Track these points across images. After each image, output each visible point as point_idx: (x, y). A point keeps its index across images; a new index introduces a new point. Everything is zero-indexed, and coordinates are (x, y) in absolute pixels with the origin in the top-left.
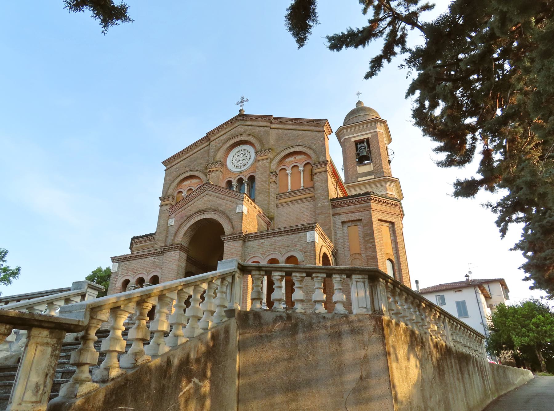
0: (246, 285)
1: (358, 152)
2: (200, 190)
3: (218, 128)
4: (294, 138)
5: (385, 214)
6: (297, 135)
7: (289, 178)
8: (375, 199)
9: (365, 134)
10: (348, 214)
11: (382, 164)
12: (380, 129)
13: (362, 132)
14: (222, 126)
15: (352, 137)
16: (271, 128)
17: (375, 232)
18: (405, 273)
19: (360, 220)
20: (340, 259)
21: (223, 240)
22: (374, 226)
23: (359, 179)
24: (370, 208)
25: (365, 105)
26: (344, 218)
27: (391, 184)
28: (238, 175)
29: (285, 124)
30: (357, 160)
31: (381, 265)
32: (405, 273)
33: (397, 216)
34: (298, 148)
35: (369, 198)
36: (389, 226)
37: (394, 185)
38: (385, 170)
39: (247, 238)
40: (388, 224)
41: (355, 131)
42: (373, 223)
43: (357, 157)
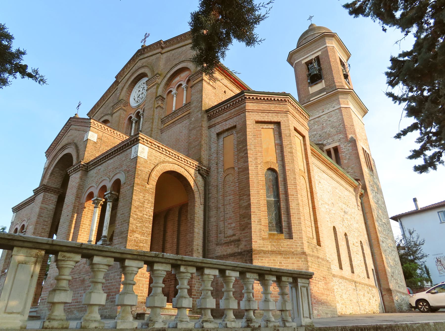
0: (192, 219)
1: (310, 72)
2: (66, 127)
3: (123, 69)
4: (178, 56)
5: (266, 113)
6: (181, 52)
7: (175, 98)
8: (251, 97)
9: (315, 53)
10: (223, 123)
11: (334, 78)
12: (331, 44)
13: (312, 52)
14: (126, 66)
15: (302, 60)
16: (162, 54)
17: (249, 137)
18: (291, 184)
19: (235, 127)
20: (212, 178)
21: (68, 173)
22: (248, 130)
23: (311, 100)
24: (244, 109)
25: (317, 25)
26: (219, 129)
27: (345, 96)
28: (136, 109)
29: (173, 45)
30: (309, 81)
31: (254, 177)
32: (291, 184)
33: (285, 114)
34: (180, 65)
35: (243, 98)
36: (273, 127)
37: (349, 97)
38: (337, 84)
39: (89, 167)
40: (272, 126)
41: (305, 53)
42: (247, 127)
43: (309, 78)
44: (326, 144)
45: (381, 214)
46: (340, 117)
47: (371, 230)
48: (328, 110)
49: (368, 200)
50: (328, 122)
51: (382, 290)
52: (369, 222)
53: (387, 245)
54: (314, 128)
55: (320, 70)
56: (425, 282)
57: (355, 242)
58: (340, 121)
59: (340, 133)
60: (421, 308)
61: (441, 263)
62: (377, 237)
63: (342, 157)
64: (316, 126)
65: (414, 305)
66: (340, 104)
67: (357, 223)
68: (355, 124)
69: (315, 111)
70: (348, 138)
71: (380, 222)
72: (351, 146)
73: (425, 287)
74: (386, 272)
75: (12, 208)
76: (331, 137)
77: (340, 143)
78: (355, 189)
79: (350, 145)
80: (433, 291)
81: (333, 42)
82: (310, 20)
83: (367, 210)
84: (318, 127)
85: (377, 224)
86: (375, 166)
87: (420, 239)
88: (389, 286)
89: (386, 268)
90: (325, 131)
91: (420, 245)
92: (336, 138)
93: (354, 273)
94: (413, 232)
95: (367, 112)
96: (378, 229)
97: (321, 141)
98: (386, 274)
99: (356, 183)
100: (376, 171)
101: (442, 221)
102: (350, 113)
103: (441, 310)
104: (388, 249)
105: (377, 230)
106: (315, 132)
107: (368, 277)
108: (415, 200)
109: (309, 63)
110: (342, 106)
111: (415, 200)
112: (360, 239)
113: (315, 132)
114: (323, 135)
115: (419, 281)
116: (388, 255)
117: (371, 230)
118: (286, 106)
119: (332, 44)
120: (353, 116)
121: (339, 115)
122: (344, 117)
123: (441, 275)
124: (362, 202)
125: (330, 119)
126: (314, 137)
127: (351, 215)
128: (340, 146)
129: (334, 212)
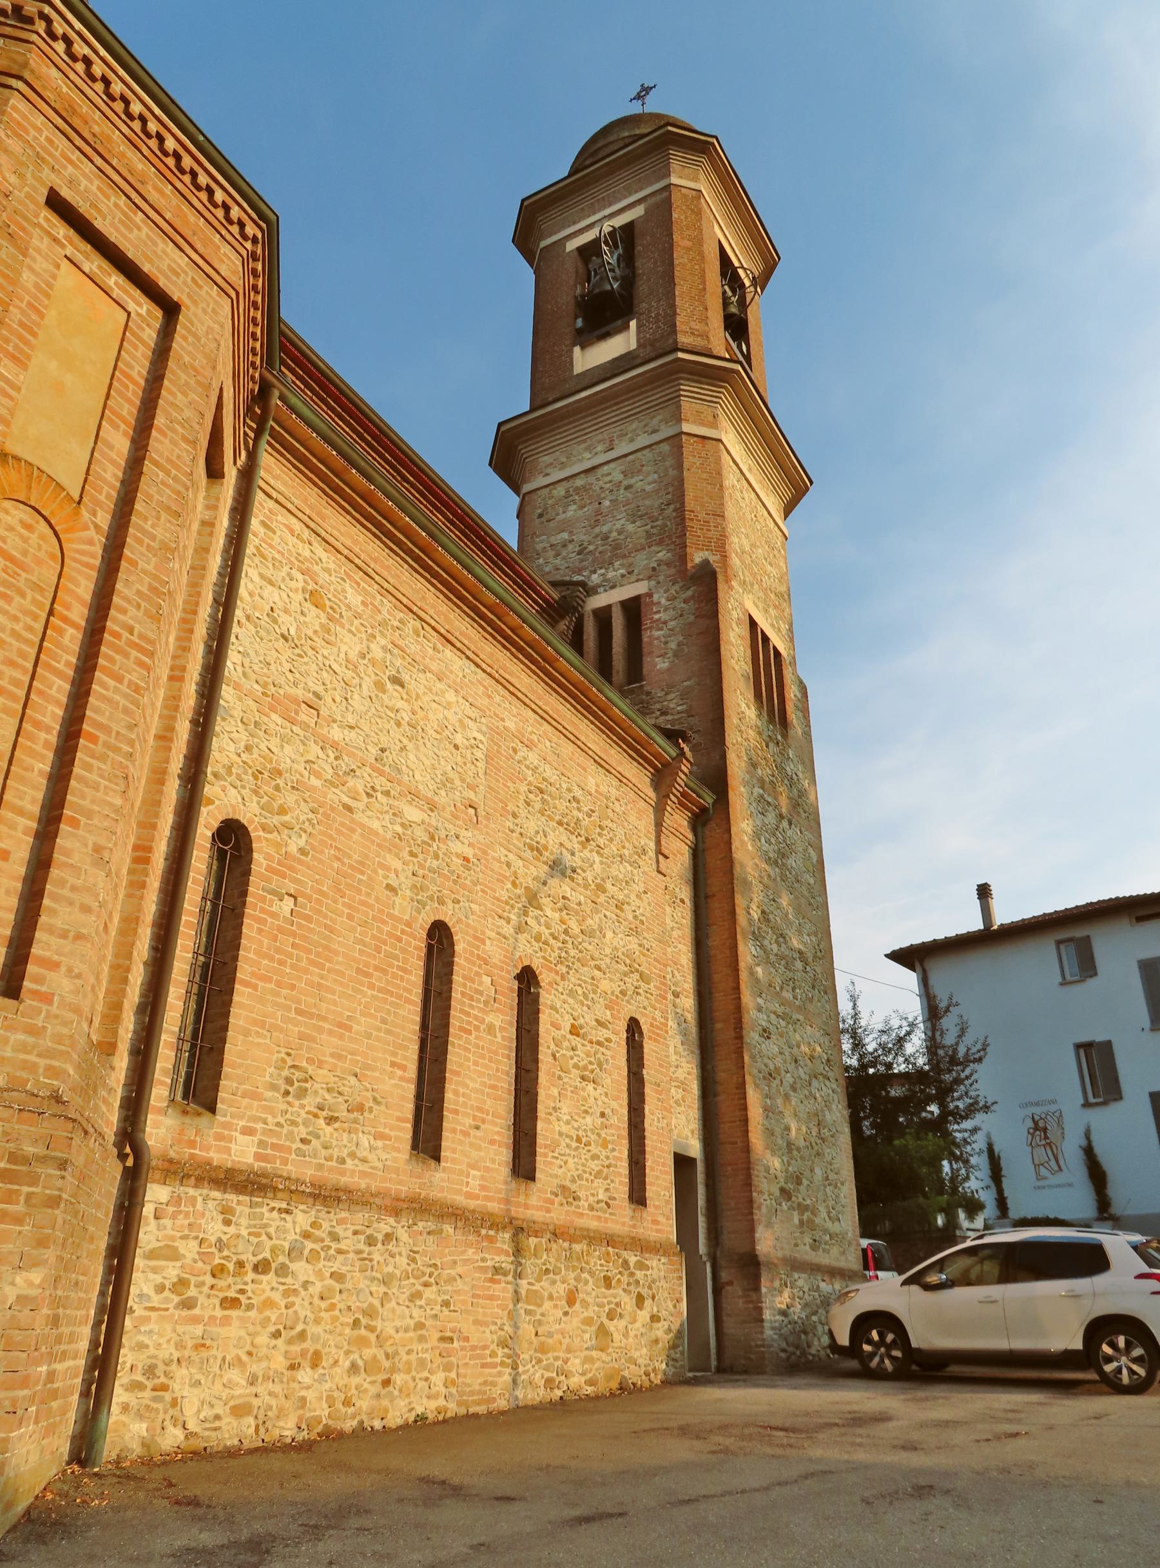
13: (610, 205)
27: (706, 390)
30: (579, 323)
44: (599, 586)
45: (790, 910)
46: (672, 473)
47: (716, 977)
48: (632, 441)
49: (726, 836)
50: (622, 495)
51: (722, 1262)
52: (715, 940)
53: (787, 1051)
54: (562, 516)
55: (629, 282)
56: (962, 1215)
57: (588, 1019)
58: (670, 489)
59: (660, 542)
60: (872, 1355)
61: (1046, 1138)
62: (738, 1008)
63: (651, 643)
64: (574, 507)
65: (844, 1340)
66: (679, 420)
67: (634, 931)
68: (730, 511)
69: (579, 443)
70: (689, 565)
71: (775, 947)
72: (693, 597)
73: (958, 1233)
74: (749, 1176)
75: (1121, 1098)
76: (624, 557)
77: (653, 583)
78: (661, 776)
79: (689, 593)
80: (933, 1278)
81: (702, 176)
82: (640, 102)
83: (715, 884)
84: (580, 513)
85: (747, 952)
86: (805, 711)
87: (968, 1039)
88: (753, 1242)
89: (754, 1156)
90: (605, 529)
91: (967, 1061)
92: (642, 561)
93: (531, 1177)
94: (947, 1010)
95: (807, 489)
96: (752, 973)
97: (579, 571)
98: (748, 1184)
99: (667, 750)
100: (807, 734)
101: (1068, 977)
102: (718, 460)
103: (954, 1369)
104: (791, 1067)
105: (744, 975)
106: (565, 535)
107: (638, 1196)
108: (984, 892)
109: (589, 251)
110: (686, 427)
111: (984, 892)
112: (629, 1010)
113: (565, 535)
114: (591, 548)
115: (942, 1210)
116: (787, 1097)
117: (719, 975)
118: (19, 48)
119: (695, 179)
120: (731, 479)
121: (668, 464)
122: (685, 472)
123: (1041, 1183)
124: (701, 846)
125: (632, 481)
126: (557, 555)
127: (601, 888)
128: (650, 595)
129: (469, 852)
